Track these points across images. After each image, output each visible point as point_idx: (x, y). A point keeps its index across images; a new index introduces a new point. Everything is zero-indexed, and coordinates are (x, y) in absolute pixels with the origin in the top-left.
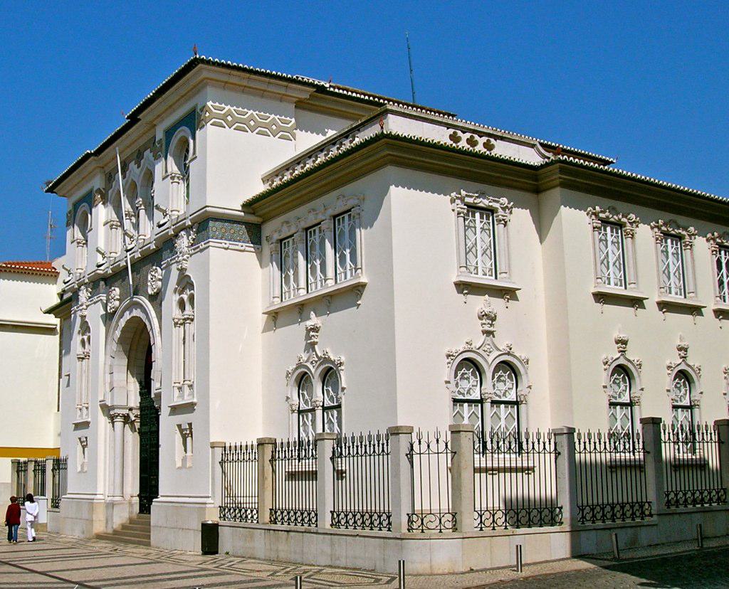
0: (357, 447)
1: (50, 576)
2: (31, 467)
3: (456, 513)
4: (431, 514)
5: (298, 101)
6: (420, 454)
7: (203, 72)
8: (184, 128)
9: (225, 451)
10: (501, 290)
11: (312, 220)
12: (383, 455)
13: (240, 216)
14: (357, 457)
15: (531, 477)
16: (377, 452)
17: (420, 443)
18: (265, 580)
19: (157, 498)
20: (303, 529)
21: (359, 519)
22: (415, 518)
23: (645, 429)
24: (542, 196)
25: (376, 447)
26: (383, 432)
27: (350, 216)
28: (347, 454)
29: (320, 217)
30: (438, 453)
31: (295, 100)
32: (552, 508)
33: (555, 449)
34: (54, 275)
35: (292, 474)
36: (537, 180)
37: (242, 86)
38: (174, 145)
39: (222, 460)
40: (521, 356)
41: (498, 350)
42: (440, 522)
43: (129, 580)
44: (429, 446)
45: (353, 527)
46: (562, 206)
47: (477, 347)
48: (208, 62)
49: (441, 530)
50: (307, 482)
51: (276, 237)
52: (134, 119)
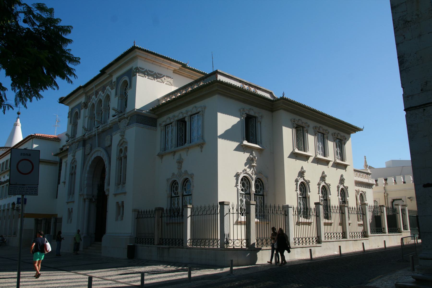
2: (43, 222)
4: (237, 240)
5: (174, 70)
6: (233, 213)
7: (138, 52)
8: (126, 77)
9: (139, 213)
10: (258, 149)
11: (168, 122)
19: (105, 234)
26: (154, 210)
27: (172, 125)
28: (147, 217)
29: (172, 120)
31: (173, 69)
33: (285, 213)
37: (152, 61)
38: (121, 84)
39: (137, 217)
42: (242, 243)
45: (178, 245)
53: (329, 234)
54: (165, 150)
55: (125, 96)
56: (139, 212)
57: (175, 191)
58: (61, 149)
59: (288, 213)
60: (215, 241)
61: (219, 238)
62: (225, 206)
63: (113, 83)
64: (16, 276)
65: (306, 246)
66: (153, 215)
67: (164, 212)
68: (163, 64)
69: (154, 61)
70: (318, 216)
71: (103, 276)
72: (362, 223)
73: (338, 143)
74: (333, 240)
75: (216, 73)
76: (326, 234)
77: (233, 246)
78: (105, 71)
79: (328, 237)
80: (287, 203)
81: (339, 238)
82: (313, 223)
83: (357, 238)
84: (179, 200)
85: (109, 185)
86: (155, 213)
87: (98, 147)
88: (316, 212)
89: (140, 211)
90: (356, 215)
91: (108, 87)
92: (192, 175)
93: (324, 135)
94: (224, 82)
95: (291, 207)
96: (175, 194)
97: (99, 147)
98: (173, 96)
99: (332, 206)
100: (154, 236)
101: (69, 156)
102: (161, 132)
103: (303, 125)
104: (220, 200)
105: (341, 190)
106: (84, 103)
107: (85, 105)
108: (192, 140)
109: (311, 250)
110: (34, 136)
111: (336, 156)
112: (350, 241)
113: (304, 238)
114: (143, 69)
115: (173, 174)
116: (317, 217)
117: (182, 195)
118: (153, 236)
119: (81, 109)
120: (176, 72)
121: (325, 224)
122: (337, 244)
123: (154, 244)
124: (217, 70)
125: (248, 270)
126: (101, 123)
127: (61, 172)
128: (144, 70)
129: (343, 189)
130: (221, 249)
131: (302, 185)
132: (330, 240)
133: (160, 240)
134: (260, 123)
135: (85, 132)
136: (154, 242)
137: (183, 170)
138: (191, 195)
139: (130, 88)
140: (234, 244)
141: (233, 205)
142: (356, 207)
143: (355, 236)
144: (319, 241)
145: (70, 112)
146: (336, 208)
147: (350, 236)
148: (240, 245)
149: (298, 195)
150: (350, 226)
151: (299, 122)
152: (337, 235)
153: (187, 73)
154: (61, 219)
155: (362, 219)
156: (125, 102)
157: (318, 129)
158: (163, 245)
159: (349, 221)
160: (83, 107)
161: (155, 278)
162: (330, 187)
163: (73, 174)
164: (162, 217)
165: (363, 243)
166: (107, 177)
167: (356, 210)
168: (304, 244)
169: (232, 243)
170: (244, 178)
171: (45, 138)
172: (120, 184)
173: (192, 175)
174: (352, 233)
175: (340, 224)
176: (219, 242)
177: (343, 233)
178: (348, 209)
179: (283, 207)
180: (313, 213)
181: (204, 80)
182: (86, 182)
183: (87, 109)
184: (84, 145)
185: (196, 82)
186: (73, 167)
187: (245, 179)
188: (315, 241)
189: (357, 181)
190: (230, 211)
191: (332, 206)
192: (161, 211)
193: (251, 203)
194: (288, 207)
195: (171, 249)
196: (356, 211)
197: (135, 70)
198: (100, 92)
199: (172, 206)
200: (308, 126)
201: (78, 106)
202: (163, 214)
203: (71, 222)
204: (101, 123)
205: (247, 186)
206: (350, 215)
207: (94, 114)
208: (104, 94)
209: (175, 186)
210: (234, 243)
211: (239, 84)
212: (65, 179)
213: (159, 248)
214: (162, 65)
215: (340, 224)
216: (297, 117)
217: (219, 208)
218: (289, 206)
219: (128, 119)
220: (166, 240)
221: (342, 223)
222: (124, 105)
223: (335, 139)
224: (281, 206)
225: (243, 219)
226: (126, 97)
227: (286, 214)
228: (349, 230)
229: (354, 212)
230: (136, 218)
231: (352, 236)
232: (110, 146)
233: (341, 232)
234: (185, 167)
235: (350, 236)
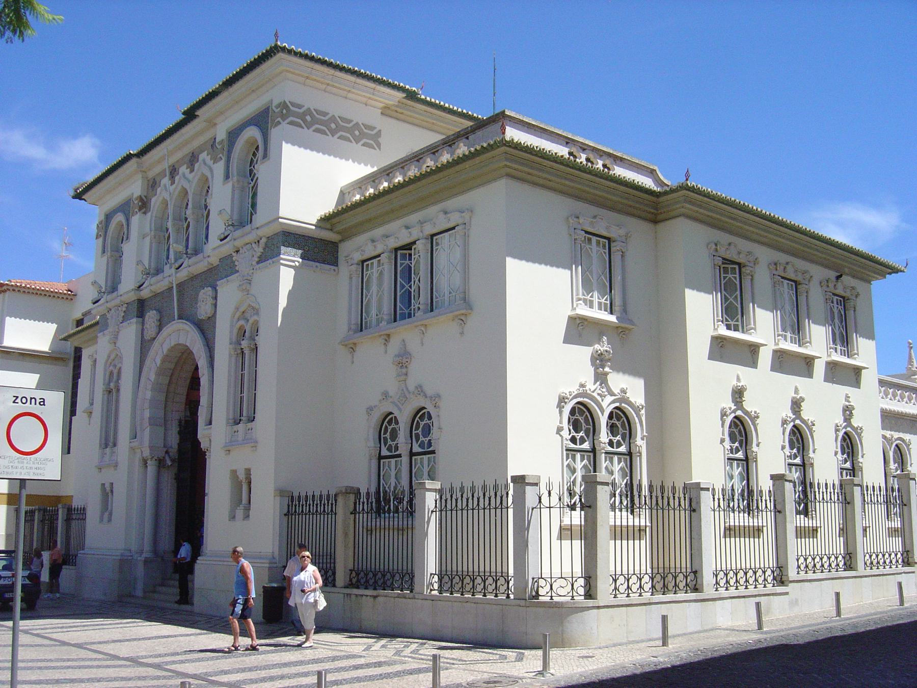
1: (51, 639)
3: (590, 577)
4: (562, 578)
5: (385, 107)
6: (550, 507)
9: (292, 502)
13: (312, 229)
14: (324, 515)
16: (312, 511)
18: (361, 657)
22: (542, 582)
23: (775, 486)
24: (661, 226)
30: (550, 507)
31: (382, 105)
32: (726, 571)
34: (69, 297)
35: (758, 530)
36: (656, 209)
39: (288, 511)
40: (636, 402)
41: (612, 394)
42: (573, 588)
43: (263, 674)
47: (592, 390)
48: (290, 52)
49: (573, 597)
50: (897, 538)
51: (358, 257)
52: (190, 115)
53: (810, 559)
54: (361, 330)
55: (252, 180)
56: (292, 497)
57: (389, 440)
58: (79, 322)
59: (699, 503)
60: (502, 581)
61: (511, 572)
62: (528, 488)
63: (217, 145)
64: (19, 672)
65: (747, 593)
66: (324, 508)
67: (362, 500)
68: (353, 93)
69: (328, 85)
70: (779, 511)
71: (206, 674)
72: (899, 526)
73: (837, 307)
74: (819, 575)
75: (500, 119)
76: (802, 560)
77: (549, 594)
78: (196, 113)
79: (807, 566)
80: (697, 477)
81: (837, 569)
82: (765, 529)
83: (884, 568)
84: (399, 466)
85: (210, 423)
86: (336, 502)
87: (178, 319)
88: (775, 501)
89: (296, 495)
90: (883, 506)
91: (204, 156)
92: (436, 398)
93: (799, 287)
94: (524, 144)
95: (708, 489)
96: (389, 449)
97: (182, 319)
98: (383, 180)
99: (818, 483)
100: (334, 563)
101: (99, 340)
102: (351, 278)
103: (742, 259)
104: (514, 469)
105: (843, 436)
106: (140, 198)
107: (144, 204)
108: (436, 302)
109: (758, 605)
110: (8, 287)
112: (866, 576)
114: (300, 107)
115: (386, 395)
116: (777, 513)
117: (409, 454)
118: (332, 561)
119: (133, 215)
120: (388, 112)
121: (802, 533)
122: (830, 588)
123: (334, 586)
124: (504, 111)
125: (590, 659)
126: (186, 253)
127: (77, 383)
128: (301, 111)
129: (850, 434)
130: (518, 602)
131: (736, 426)
132: (810, 576)
133: (351, 573)
135: (144, 276)
136: (334, 580)
137: (411, 384)
138: (433, 452)
139: (263, 159)
140: (551, 589)
141: (549, 484)
142: (883, 485)
143: (878, 563)
144: (781, 579)
145: (101, 223)
146: (830, 489)
147: (866, 564)
148: (568, 593)
149: (727, 452)
150: (865, 538)
151: (728, 252)
152: (831, 561)
153: (420, 114)
154: (83, 511)
155: (900, 514)
156: (251, 195)
157: (781, 268)
158: (358, 587)
159: (864, 522)
160: (137, 210)
161: (344, 680)
162: (814, 429)
163: (112, 392)
164: (354, 512)
165: (900, 584)
166: (204, 401)
167: (883, 492)
168: (742, 588)
170: (578, 407)
171: (35, 292)
172: (240, 420)
173: (436, 398)
174: (871, 556)
176: (511, 583)
177: (848, 557)
178: (862, 490)
179: (684, 488)
180: (766, 503)
181: (467, 138)
182: (147, 414)
183: (149, 214)
184: (141, 314)
185: (450, 142)
186: (111, 373)
188: (770, 579)
189: (886, 409)
190: (542, 500)
191: (818, 484)
192: (352, 497)
193: (598, 480)
194: (698, 487)
195: (380, 599)
196: (884, 495)
197: (279, 109)
198: (183, 169)
199: (382, 481)
200: (756, 261)
201: (125, 208)
202: (358, 506)
203: (110, 520)
204: (186, 253)
205: (587, 428)
206: (866, 505)
207: (167, 230)
208: (193, 173)
209: (390, 428)
210: (551, 586)
211: (562, 151)
212: (92, 404)
213: (349, 595)
214: (350, 95)
216: (725, 238)
217: (511, 492)
218: (702, 486)
219: (259, 245)
220: (366, 575)
221: (846, 530)
222: (250, 206)
223: (827, 297)
224: (679, 486)
225: (577, 518)
226: (252, 184)
227: (694, 509)
228: (863, 546)
229: (877, 498)
230: (285, 515)
231: (872, 563)
232: (212, 319)
233: (842, 552)
234: (418, 374)
235: (866, 564)
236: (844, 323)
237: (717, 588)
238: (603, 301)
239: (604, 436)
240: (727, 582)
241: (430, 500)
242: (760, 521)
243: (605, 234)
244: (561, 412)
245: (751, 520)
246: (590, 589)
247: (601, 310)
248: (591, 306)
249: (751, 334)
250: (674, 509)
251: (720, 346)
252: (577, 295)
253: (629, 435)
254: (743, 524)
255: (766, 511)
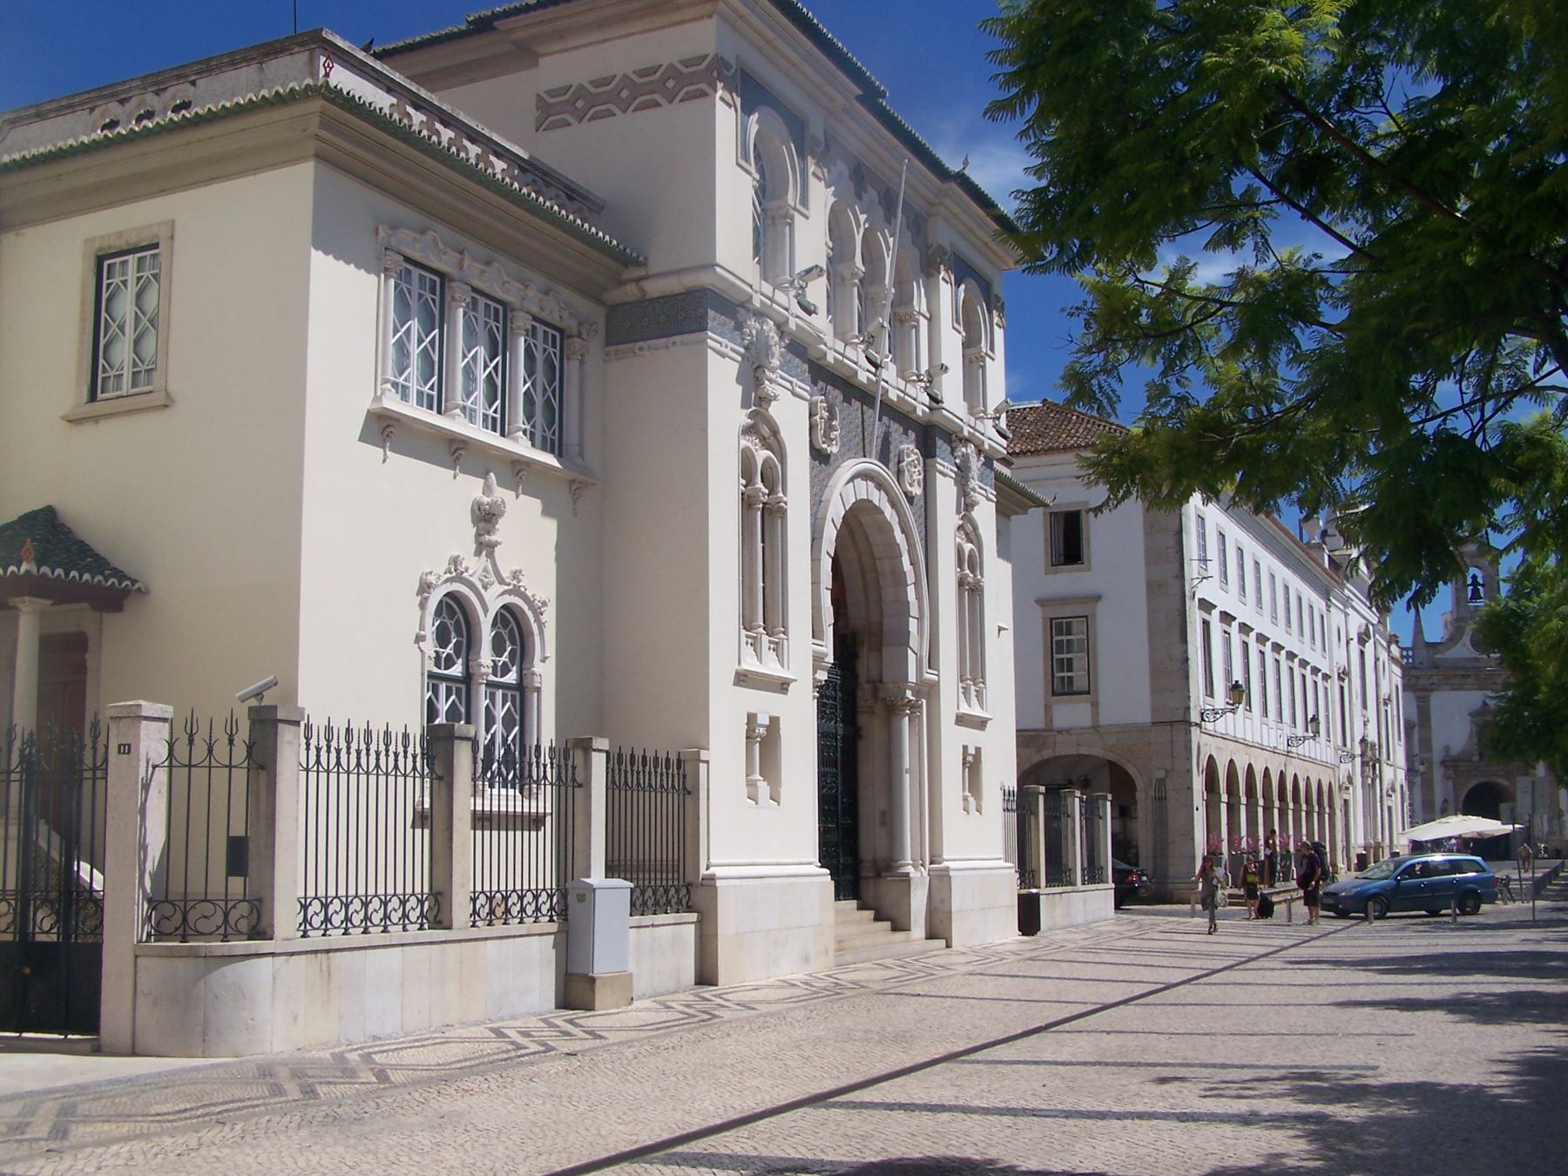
0: (396, 755)
6: (190, 766)
12: (396, 776)
15: (541, 833)
17: (191, 742)
20: (522, 929)
21: (544, 903)
25: (641, 777)
41: (502, 581)
44: (210, 751)
46: (1441, 583)
94: (348, 93)
111: (384, 373)
113: (514, 895)
131: (505, 623)
134: (582, 363)
169: (233, 917)
175: (422, 819)
187: (505, 617)
215: (422, 819)
236: (557, 383)
237: (305, 932)
238: (426, 389)
239: (486, 656)
240: (348, 919)
241: (152, 743)
242: (541, 804)
243: (500, 295)
244: (422, 606)
245: (526, 803)
246: (259, 916)
247: (422, 406)
248: (472, 420)
249: (454, 419)
250: (387, 774)
251: (385, 434)
252: (384, 373)
253: (522, 656)
254: (489, 809)
255: (338, 773)
